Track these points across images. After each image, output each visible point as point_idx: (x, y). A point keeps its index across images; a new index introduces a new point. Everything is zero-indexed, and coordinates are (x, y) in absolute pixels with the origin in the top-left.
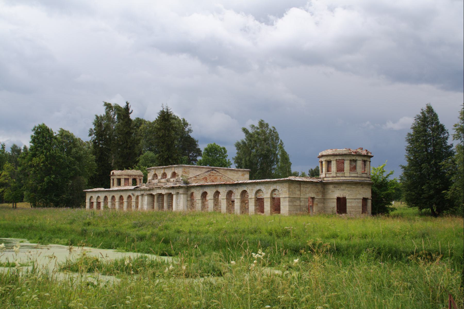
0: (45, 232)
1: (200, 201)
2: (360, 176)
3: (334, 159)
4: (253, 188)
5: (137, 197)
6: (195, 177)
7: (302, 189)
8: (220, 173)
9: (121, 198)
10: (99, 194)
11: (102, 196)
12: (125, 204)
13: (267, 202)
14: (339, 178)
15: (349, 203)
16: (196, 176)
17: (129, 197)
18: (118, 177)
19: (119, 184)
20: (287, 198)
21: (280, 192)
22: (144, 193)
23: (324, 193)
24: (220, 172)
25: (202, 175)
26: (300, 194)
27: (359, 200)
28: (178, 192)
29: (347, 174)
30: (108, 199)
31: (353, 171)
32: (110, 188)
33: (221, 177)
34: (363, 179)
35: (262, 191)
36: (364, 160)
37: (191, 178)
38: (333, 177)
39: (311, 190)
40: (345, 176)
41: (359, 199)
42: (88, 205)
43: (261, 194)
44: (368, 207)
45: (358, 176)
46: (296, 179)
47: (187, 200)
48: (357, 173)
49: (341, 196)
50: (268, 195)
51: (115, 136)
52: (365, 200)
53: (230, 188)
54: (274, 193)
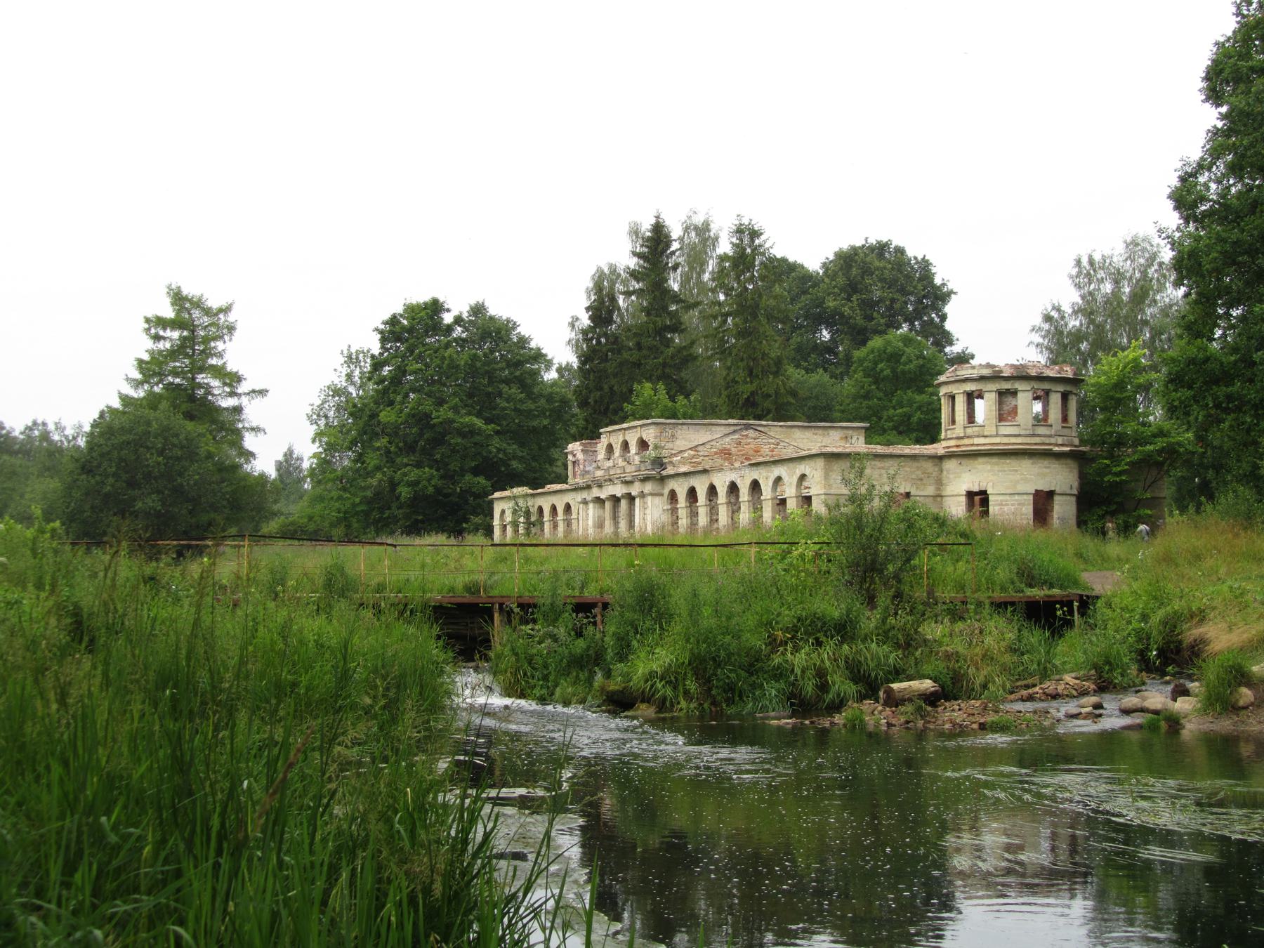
0: (153, 668)
2: (1028, 432)
6: (694, 448)
8: (770, 437)
24: (772, 434)
25: (714, 443)
27: (1025, 497)
32: (934, 439)
34: (1037, 440)
37: (681, 452)
38: (959, 438)
40: (986, 433)
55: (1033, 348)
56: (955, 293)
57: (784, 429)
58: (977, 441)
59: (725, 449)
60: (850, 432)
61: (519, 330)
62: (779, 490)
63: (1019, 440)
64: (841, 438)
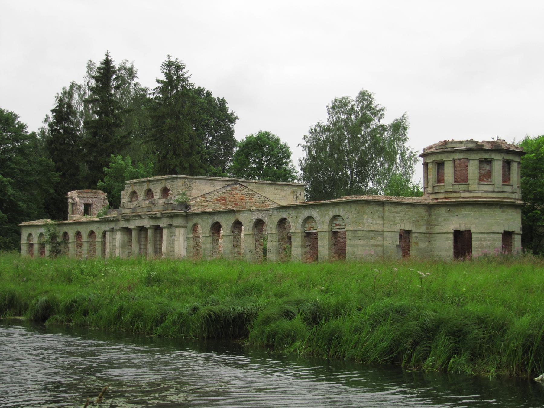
1: (209, 240)
2: (499, 190)
3: (448, 157)
4: (299, 215)
5: (104, 234)
6: (203, 196)
7: (387, 214)
8: (250, 190)
12: (85, 247)
13: (322, 239)
15: (476, 241)
16: (204, 194)
17: (92, 233)
20: (297, 234)
21: (346, 221)
22: (115, 225)
24: (251, 188)
25: (215, 193)
26: (384, 224)
27: (497, 235)
28: (171, 223)
31: (486, 181)
33: (251, 196)
34: (505, 195)
35: (313, 219)
36: (507, 160)
37: (195, 198)
38: (446, 192)
39: (404, 217)
40: (470, 190)
41: (496, 233)
42: (24, 248)
44: (514, 248)
45: (496, 190)
47: (188, 238)
48: (494, 184)
49: (462, 228)
50: (325, 227)
51: (382, 188)
52: (507, 235)
54: (335, 222)
55: (300, 148)
56: (238, 119)
57: (258, 185)
58: (463, 195)
59: (222, 197)
60: (296, 189)
61: (19, 120)
62: (307, 226)
63: (494, 195)
64: (291, 193)
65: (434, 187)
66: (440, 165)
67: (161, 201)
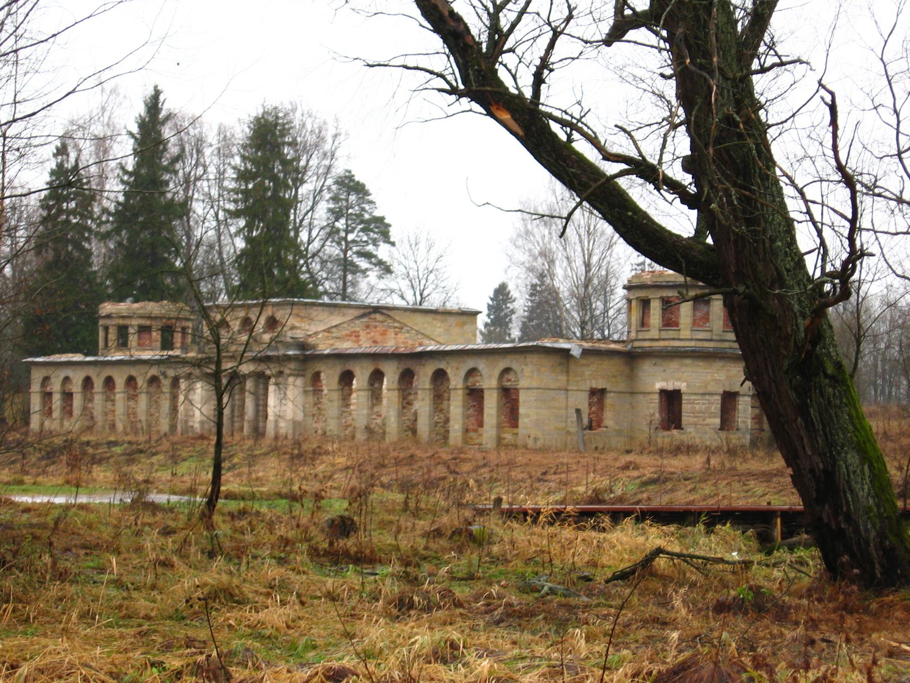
2: (718, 338)
4: (461, 365)
8: (395, 321)
9: (131, 381)
10: (69, 372)
11: (77, 377)
12: (98, 399)
14: (666, 343)
16: (329, 328)
18: (121, 322)
19: (123, 343)
23: (631, 376)
24: (397, 318)
25: (345, 325)
29: (685, 333)
30: (95, 385)
43: (478, 378)
45: (715, 338)
46: (557, 345)
50: (494, 383)
53: (409, 364)
65: (637, 331)
66: (645, 303)
67: (267, 337)
